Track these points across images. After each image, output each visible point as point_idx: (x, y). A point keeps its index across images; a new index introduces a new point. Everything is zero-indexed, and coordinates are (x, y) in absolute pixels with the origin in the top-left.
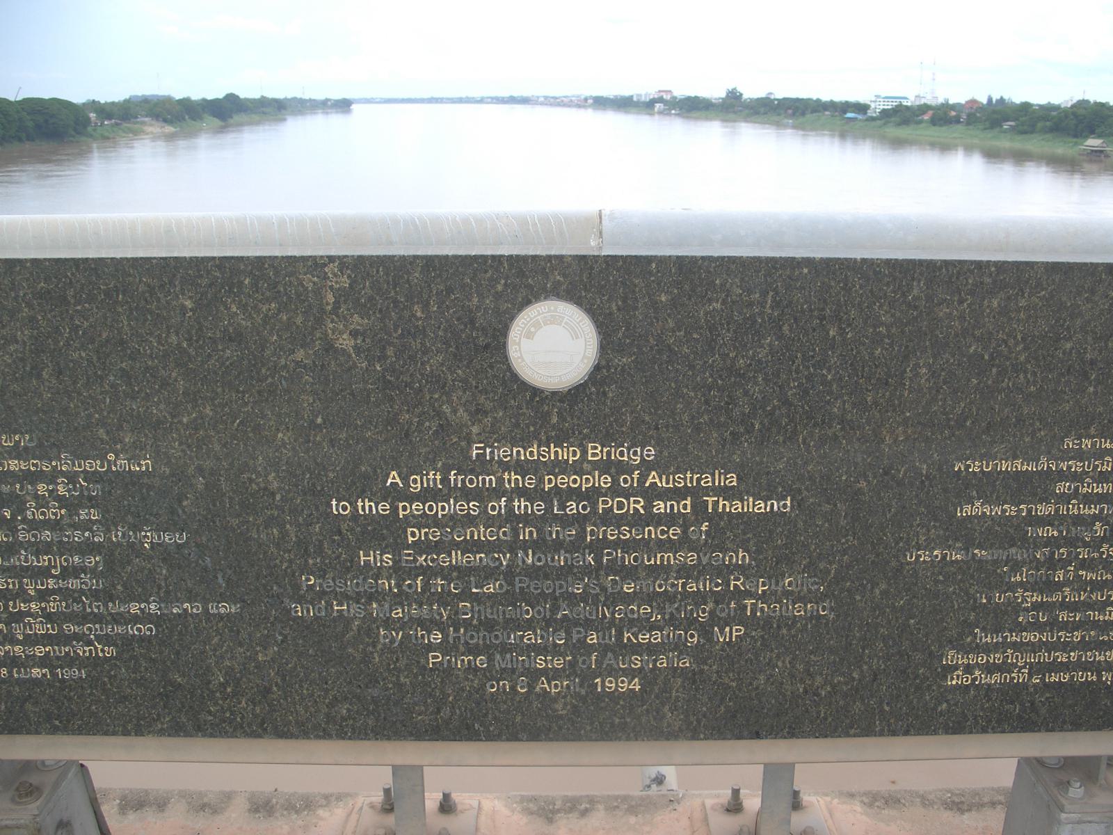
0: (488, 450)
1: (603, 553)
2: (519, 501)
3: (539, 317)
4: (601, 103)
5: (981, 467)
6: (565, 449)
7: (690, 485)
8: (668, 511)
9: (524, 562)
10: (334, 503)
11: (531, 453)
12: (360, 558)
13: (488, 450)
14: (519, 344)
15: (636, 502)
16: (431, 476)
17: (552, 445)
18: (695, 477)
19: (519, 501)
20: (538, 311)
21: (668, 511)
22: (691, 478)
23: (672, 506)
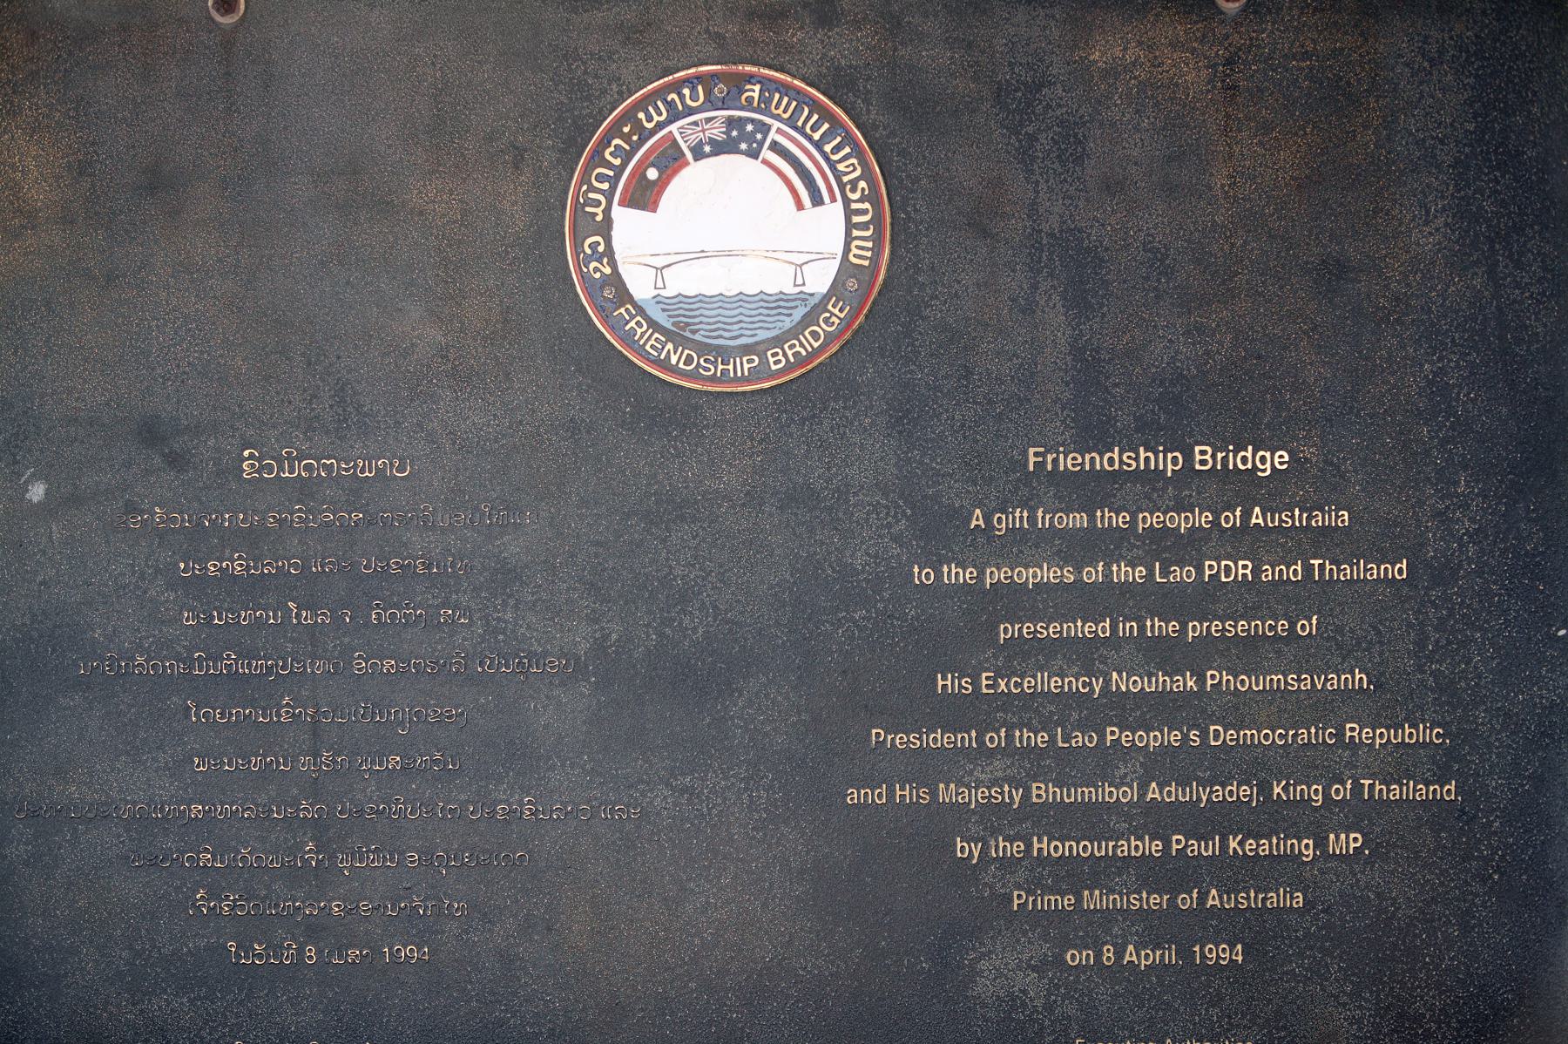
0: (1050, 458)
1: (1271, 909)
2: (1152, 620)
3: (674, 128)
4: (645, 265)
5: (1389, 791)
6: (1161, 455)
7: (1150, 635)
8: (1073, 790)
9: (1118, 687)
10: (916, 570)
11: (1111, 460)
12: (1110, 626)
13: (1050, 458)
14: (606, 228)
15: (1245, 567)
16: (1017, 514)
17: (1142, 449)
18: (1260, 896)
19: (1152, 620)
20: (670, 105)
21: (1073, 790)
22: (1256, 898)
23: (1069, 796)
